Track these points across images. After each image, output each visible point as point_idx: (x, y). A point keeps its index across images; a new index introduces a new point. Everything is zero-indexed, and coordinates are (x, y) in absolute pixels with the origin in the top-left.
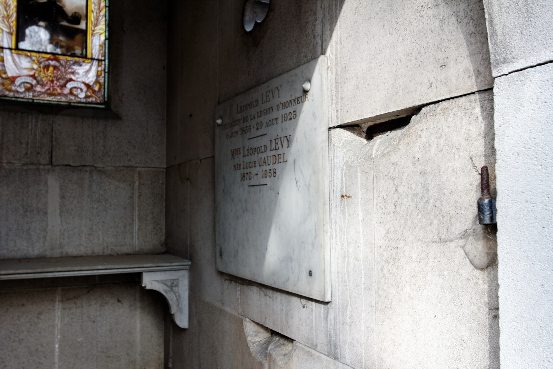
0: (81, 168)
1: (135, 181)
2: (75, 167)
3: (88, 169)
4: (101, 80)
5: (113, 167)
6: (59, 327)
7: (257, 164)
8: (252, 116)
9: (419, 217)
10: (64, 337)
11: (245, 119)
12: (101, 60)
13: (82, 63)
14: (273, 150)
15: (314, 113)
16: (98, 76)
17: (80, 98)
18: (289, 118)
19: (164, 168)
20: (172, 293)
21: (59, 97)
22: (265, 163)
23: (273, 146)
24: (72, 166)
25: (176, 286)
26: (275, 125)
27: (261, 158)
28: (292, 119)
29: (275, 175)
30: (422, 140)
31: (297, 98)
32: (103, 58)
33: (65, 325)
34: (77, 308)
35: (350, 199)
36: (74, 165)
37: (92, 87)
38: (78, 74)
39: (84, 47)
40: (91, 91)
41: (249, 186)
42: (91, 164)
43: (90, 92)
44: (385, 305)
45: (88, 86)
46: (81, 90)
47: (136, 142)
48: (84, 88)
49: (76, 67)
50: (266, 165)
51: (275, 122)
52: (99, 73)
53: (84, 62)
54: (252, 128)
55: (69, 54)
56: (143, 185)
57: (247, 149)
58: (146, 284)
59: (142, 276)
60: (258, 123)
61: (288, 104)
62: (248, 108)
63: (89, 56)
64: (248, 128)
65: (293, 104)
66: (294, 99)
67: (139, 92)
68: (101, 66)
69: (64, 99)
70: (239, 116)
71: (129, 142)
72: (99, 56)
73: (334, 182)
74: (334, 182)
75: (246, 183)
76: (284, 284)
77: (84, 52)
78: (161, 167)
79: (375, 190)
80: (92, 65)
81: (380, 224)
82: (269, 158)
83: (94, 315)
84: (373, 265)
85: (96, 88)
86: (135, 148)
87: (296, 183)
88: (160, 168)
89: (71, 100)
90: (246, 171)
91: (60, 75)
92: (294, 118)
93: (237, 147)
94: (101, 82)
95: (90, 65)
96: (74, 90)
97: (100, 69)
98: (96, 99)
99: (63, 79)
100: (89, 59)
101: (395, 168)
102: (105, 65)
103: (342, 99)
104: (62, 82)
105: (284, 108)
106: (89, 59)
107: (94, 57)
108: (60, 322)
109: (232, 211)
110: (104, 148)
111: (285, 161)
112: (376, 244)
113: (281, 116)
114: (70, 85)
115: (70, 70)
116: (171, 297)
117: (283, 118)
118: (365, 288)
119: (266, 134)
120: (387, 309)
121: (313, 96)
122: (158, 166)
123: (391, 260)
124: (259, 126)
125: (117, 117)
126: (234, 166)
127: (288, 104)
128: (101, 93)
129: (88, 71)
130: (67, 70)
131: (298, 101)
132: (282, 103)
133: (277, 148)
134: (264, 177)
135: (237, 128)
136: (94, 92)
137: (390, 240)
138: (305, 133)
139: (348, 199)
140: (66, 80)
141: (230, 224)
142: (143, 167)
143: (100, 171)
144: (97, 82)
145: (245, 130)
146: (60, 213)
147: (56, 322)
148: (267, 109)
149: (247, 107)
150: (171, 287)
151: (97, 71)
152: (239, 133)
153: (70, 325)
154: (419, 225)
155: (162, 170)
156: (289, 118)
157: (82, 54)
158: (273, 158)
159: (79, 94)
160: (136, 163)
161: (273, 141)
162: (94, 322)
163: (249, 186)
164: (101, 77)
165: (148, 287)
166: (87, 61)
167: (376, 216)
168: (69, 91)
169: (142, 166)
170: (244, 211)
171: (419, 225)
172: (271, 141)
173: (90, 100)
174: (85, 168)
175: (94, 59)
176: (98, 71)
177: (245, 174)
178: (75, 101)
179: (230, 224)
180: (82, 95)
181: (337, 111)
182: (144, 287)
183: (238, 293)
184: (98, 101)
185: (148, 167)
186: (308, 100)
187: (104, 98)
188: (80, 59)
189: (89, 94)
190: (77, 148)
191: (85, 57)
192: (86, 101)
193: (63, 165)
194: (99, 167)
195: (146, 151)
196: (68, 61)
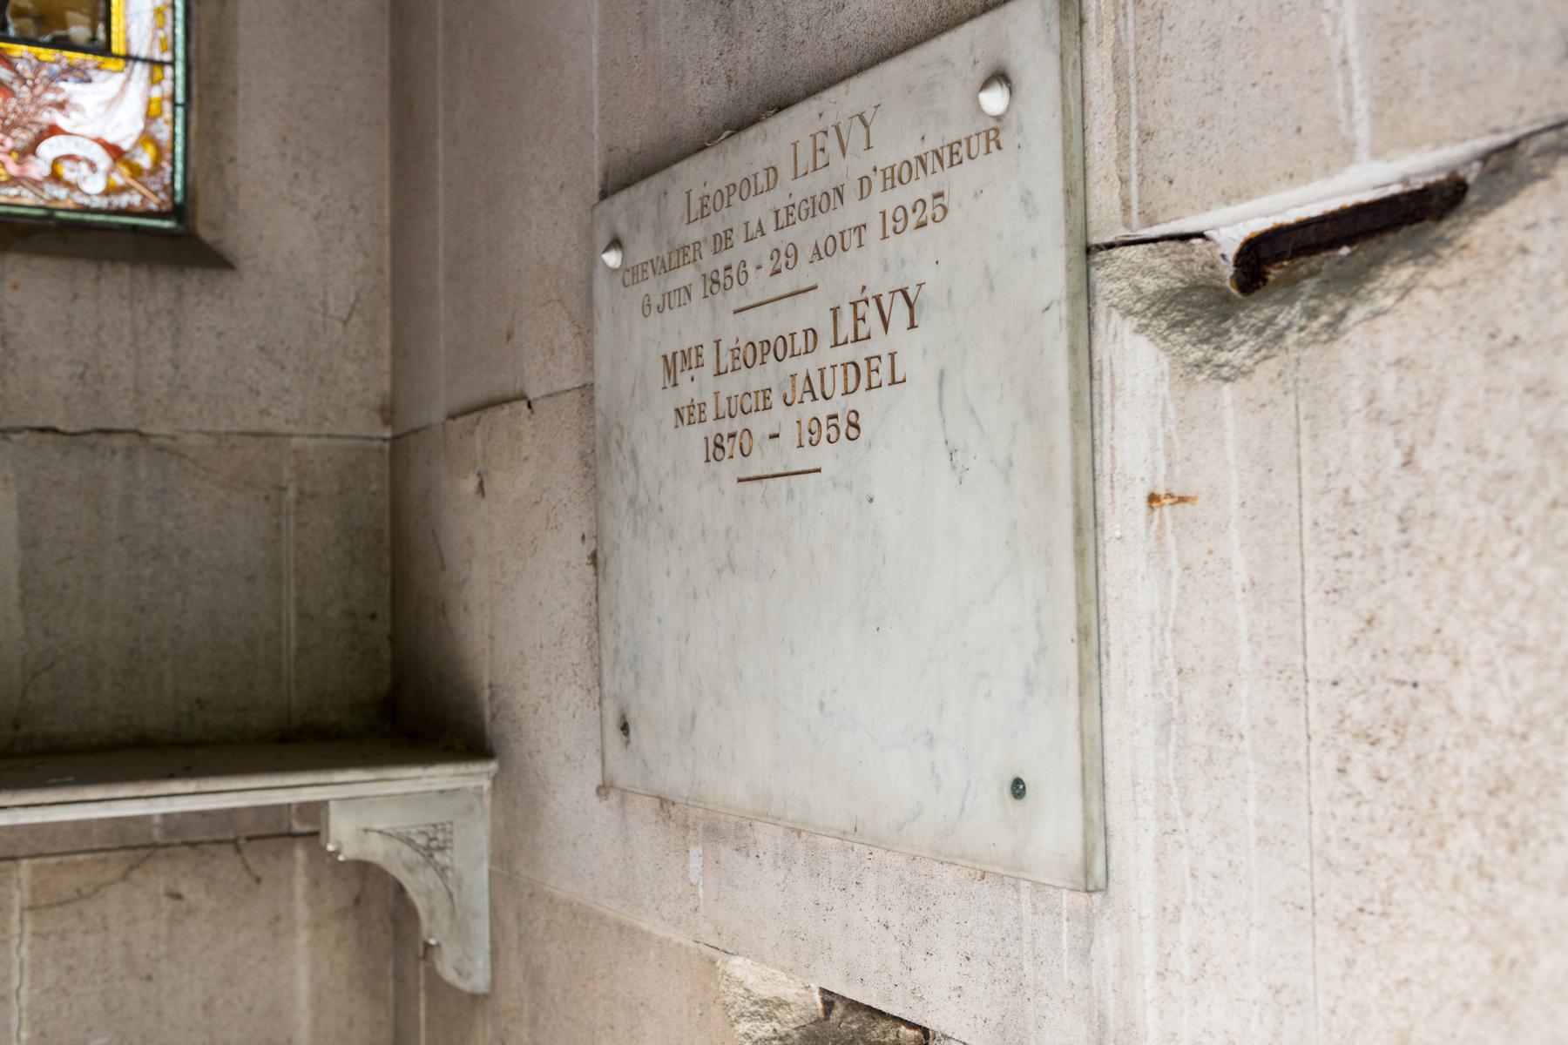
0: (93, 438)
1: (284, 484)
2: (74, 434)
3: (118, 442)
4: (161, 131)
5: (208, 434)
6: (24, 1001)
7: (775, 399)
8: (753, 227)
9: (1522, 560)
10: (42, 1034)
11: (723, 241)
12: (162, 64)
13: (92, 73)
14: (846, 343)
15: (1029, 193)
16: (150, 118)
17: (88, 195)
18: (913, 219)
19: (384, 440)
20: (430, 870)
21: (13, 192)
22: (812, 391)
23: (846, 328)
24: (64, 433)
25: (441, 849)
26: (853, 252)
27: (793, 376)
28: (930, 221)
29: (853, 432)
30: (1535, 263)
31: (951, 146)
32: (167, 57)
33: (47, 991)
34: (86, 932)
35: (1187, 506)
36: (71, 429)
37: (127, 157)
38: (77, 107)
39: (101, 14)
40: (125, 170)
41: (740, 480)
42: (130, 425)
43: (121, 175)
44: (1359, 904)
45: (116, 153)
46: (92, 166)
47: (288, 348)
48: (103, 160)
49: (70, 88)
50: (815, 399)
51: (855, 238)
52: (154, 107)
53: (98, 68)
54: (750, 268)
55: (47, 38)
56: (313, 497)
57: (733, 346)
58: (339, 843)
59: (328, 813)
60: (777, 250)
61: (911, 171)
62: (735, 199)
63: (117, 47)
64: (734, 273)
65: (930, 170)
66: (936, 152)
67: (296, 176)
68: (159, 82)
69: (28, 197)
70: (696, 232)
71: (262, 349)
72: (151, 48)
73: (1112, 447)
74: (1112, 447)
75: (730, 468)
76: (899, 830)
77: (101, 36)
78: (374, 435)
79: (1305, 468)
80: (129, 79)
81: (1333, 597)
82: (828, 373)
83: (147, 956)
84: (1302, 750)
85: (145, 160)
86: (283, 368)
87: (947, 458)
88: (370, 438)
89: (56, 199)
90: (725, 427)
91: (15, 112)
92: (790, 266)
93: (688, 342)
94: (160, 141)
95: (121, 77)
96: (67, 164)
97: (156, 92)
98: (145, 197)
99: (24, 128)
100: (117, 57)
101: (1400, 380)
102: (174, 79)
103: (1147, 135)
104: (24, 137)
105: (893, 187)
106: (117, 57)
107: (134, 51)
108: (26, 983)
109: (668, 573)
110: (176, 367)
111: (898, 378)
112: (1311, 674)
113: (880, 217)
114: (50, 149)
115: (50, 97)
116: (419, 885)
117: (890, 223)
118: (1263, 840)
119: (814, 288)
120: (1365, 918)
121: (1020, 129)
122: (366, 433)
123: (1386, 733)
124: (783, 259)
125: (214, 260)
126: (677, 410)
127: (911, 171)
128: (162, 178)
129: (113, 102)
130: (39, 97)
131: (952, 155)
132: (884, 171)
133: (861, 334)
134: (805, 442)
135: (686, 275)
136: (136, 172)
137: (1380, 653)
138: (987, 268)
139: (1179, 507)
140: (35, 129)
141: (660, 621)
142: (311, 436)
143: (161, 449)
144: (147, 137)
145: (721, 279)
146: (22, 597)
147: (15, 983)
148: (819, 194)
149: (729, 196)
150: (428, 852)
151: (145, 99)
152: (697, 292)
153: (65, 993)
154: (1523, 590)
155: (376, 444)
156: (913, 219)
157: (94, 39)
158: (846, 372)
159: (85, 178)
160: (287, 421)
161: (847, 311)
162: (149, 978)
163: (740, 480)
164: (160, 121)
165: (349, 852)
166: (111, 64)
167: (1309, 565)
168: (47, 171)
169: (309, 431)
170: (719, 571)
171: (1523, 590)
172: (835, 310)
173: (123, 201)
174: (105, 441)
175: (136, 59)
176: (149, 102)
177: (725, 437)
178: (70, 205)
179: (660, 621)
180: (93, 185)
181: (1124, 182)
182: (332, 853)
183: (695, 865)
184: (153, 206)
185: (329, 436)
186: (999, 148)
187: (173, 194)
188: (90, 57)
189: (118, 180)
190: (80, 368)
191: (105, 50)
192: (110, 204)
193: (32, 429)
194: (155, 436)
195: (322, 380)
196: (41, 63)
